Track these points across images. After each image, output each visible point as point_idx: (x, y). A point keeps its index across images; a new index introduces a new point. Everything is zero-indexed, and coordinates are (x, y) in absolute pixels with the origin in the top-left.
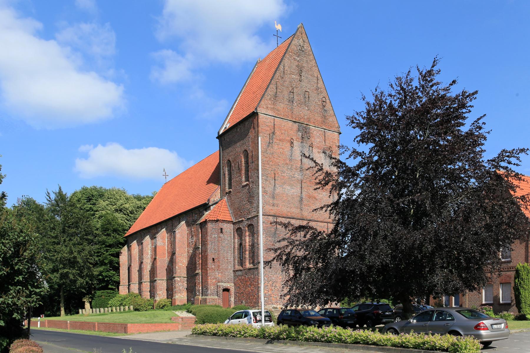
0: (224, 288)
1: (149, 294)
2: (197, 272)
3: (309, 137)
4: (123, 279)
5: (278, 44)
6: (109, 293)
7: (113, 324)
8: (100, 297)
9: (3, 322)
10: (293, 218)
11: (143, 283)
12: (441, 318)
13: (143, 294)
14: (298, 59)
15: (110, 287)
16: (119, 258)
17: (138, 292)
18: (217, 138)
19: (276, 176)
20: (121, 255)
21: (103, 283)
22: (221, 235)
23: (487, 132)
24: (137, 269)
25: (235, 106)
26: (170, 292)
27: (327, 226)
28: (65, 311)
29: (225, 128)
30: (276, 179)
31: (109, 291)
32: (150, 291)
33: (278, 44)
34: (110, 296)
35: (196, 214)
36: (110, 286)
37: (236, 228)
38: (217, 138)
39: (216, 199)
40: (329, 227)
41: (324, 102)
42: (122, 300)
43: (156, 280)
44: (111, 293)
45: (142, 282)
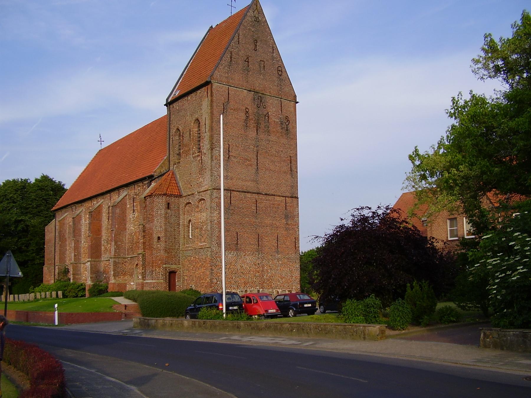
0: (171, 270)
2: (316, 308)
3: (265, 107)
5: (231, 13)
7: (60, 237)
9: (37, 288)
10: (248, 192)
14: (253, 30)
18: (165, 105)
19: (230, 147)
22: (169, 211)
23: (369, 207)
25: (185, 73)
26: (105, 275)
27: (285, 201)
29: (174, 95)
30: (230, 150)
33: (231, 13)
35: (139, 186)
37: (185, 203)
38: (165, 105)
39: (162, 171)
40: (287, 202)
41: (280, 71)
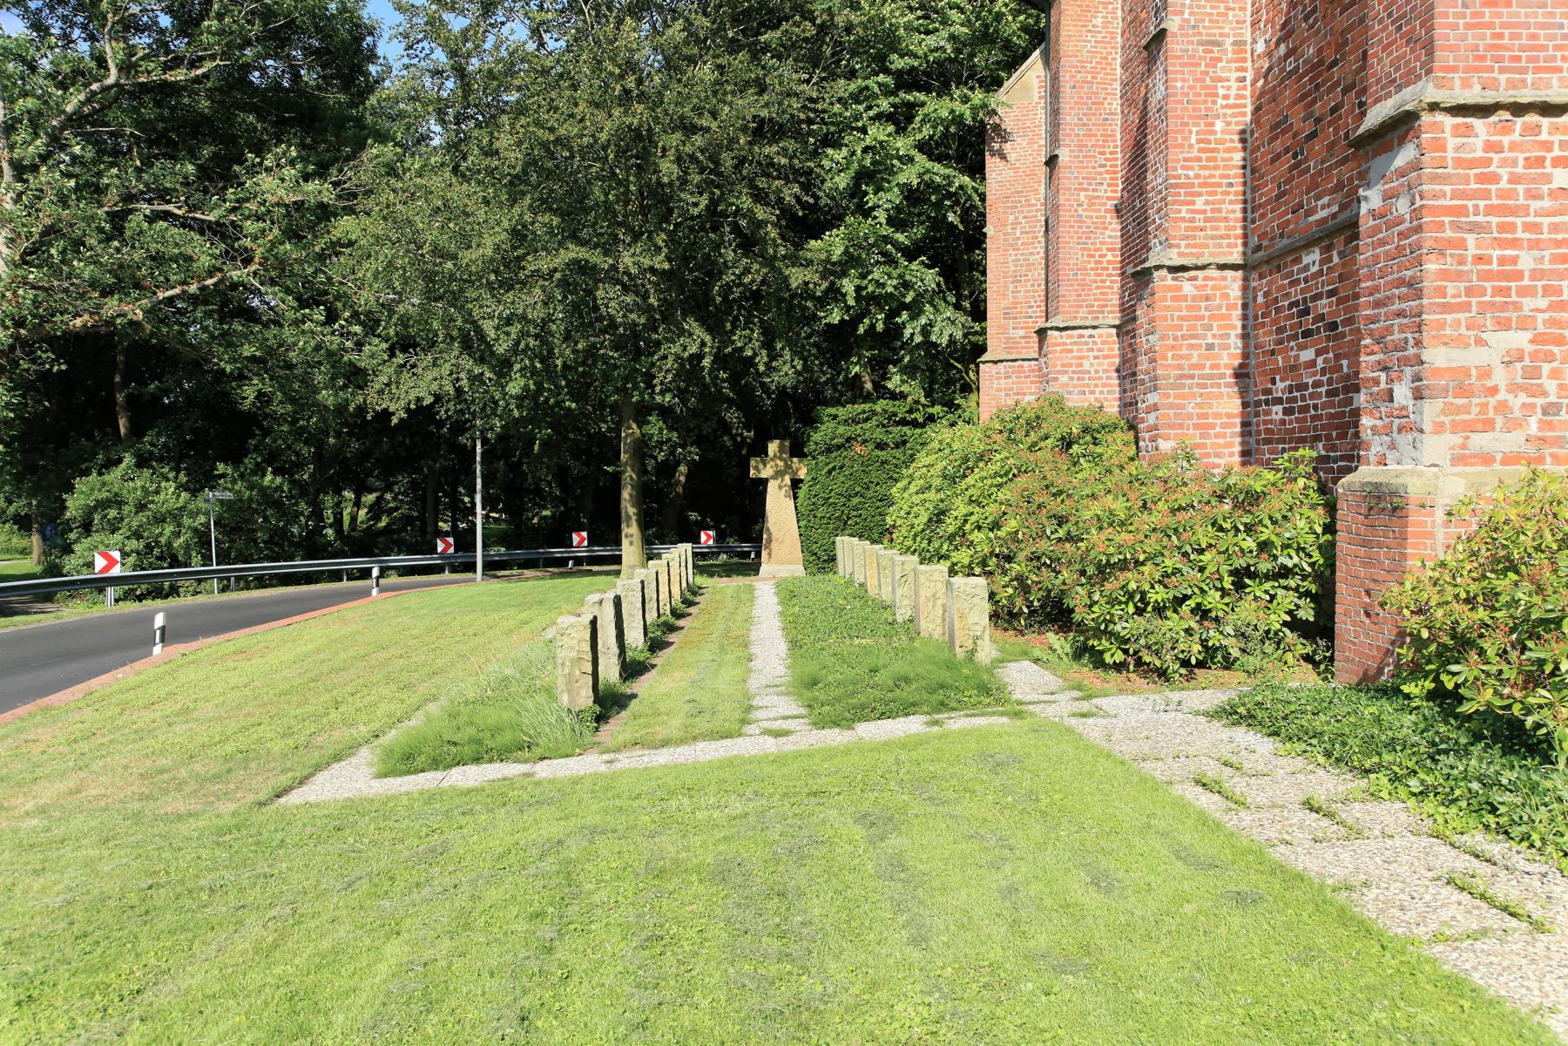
1: (1235, 405)
4: (1006, 316)
6: (903, 422)
8: (839, 447)
11: (1162, 280)
13: (1159, 405)
16: (977, 170)
17: (1112, 408)
24: (1111, 189)
28: (644, 526)
32: (1241, 375)
43: (1402, 125)
45: (1147, 273)
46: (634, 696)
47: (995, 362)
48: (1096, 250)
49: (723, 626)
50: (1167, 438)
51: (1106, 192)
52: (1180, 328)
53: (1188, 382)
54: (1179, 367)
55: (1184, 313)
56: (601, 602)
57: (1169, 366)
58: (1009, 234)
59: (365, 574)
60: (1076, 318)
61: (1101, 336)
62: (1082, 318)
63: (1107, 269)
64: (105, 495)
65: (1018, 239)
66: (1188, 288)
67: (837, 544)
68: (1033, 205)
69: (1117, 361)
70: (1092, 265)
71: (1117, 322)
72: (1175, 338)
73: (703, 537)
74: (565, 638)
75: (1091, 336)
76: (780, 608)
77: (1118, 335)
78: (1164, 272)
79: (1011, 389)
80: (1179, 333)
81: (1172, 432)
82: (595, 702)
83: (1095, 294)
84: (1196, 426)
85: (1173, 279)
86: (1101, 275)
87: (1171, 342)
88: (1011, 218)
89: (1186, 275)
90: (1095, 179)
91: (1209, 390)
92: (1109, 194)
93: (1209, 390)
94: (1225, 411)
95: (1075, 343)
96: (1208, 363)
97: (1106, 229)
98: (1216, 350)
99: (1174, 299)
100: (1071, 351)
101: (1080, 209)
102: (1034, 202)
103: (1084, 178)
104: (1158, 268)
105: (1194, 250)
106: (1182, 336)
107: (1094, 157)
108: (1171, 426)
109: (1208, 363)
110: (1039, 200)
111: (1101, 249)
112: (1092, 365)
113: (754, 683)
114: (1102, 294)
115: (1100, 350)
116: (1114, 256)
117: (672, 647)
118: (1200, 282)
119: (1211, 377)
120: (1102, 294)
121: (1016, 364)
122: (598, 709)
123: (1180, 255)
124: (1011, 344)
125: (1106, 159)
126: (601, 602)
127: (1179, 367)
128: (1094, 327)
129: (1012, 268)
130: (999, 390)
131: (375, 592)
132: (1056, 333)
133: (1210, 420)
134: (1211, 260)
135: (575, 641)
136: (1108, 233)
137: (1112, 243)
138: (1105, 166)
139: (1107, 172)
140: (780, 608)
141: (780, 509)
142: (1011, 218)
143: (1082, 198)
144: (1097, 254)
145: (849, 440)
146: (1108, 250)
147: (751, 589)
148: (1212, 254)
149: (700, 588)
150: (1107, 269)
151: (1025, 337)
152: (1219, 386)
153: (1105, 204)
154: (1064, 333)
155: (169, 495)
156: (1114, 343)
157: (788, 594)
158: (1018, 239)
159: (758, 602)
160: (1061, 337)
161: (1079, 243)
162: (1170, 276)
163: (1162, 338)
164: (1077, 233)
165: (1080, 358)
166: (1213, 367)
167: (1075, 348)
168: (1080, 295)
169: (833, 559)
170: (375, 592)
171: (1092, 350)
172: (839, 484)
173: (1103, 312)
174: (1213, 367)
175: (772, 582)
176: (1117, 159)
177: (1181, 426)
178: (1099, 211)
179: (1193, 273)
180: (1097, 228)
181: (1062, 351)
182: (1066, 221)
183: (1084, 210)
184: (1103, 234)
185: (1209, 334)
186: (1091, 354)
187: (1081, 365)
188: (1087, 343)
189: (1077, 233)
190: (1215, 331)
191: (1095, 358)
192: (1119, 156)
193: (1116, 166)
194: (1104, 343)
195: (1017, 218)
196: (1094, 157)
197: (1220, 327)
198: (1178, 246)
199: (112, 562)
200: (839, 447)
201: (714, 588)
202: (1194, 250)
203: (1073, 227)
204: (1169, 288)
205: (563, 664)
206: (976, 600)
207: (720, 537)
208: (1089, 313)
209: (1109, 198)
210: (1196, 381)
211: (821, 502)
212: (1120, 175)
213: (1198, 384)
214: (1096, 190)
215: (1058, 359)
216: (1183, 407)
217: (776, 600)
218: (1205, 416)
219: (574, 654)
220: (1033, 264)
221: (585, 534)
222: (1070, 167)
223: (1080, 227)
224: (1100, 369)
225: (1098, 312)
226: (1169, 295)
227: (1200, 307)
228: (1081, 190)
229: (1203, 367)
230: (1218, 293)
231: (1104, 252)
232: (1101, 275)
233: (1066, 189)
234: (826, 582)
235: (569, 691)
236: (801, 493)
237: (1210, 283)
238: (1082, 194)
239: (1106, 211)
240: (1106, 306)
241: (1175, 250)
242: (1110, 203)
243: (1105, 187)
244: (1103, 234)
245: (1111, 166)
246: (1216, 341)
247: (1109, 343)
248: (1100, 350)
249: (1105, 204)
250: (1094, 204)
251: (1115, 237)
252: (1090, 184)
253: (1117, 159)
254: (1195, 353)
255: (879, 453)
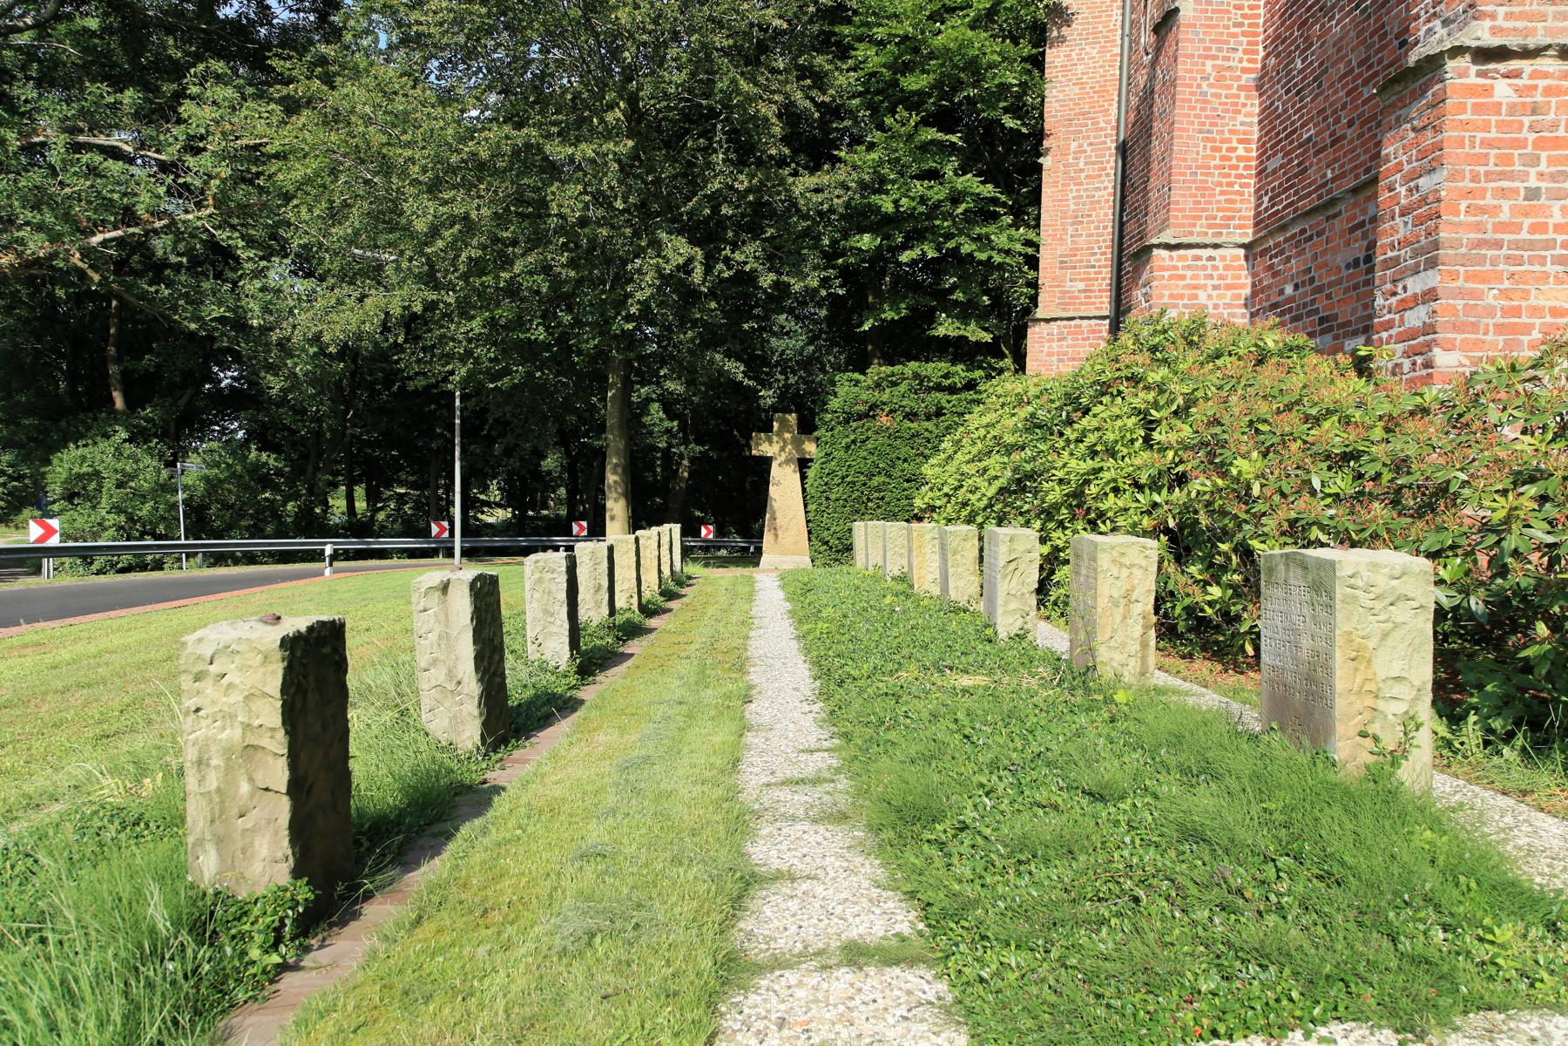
6: (939, 388)
8: (860, 417)
11: (1461, 73)
12: (531, 513)
15: (941, 331)
20: (1062, 39)
21: (895, 307)
31: (934, 369)
34: (939, 413)
36: (946, 327)
42: (1033, 424)
44: (952, 390)
46: (498, 790)
47: (1047, 321)
48: (1222, 141)
49: (708, 631)
50: (1449, 347)
51: (1241, 61)
52: (1483, 159)
53: (1490, 253)
54: (1479, 227)
55: (1493, 134)
56: (445, 588)
57: (1460, 224)
58: (1069, 165)
59: (317, 556)
60: (1191, 233)
61: (1223, 258)
62: (1199, 234)
63: (1236, 168)
64: (85, 469)
65: (1082, 171)
66: (1503, 90)
67: (855, 531)
68: (1101, 129)
69: (1248, 291)
70: (1217, 162)
71: (1247, 240)
72: (1475, 178)
73: (704, 531)
74: (208, 686)
75: (1211, 258)
76: (789, 606)
77: (1247, 258)
78: (1464, 62)
79: (1065, 354)
80: (1482, 169)
81: (1460, 337)
82: (297, 873)
83: (1218, 202)
84: (1500, 329)
85: (1480, 74)
86: (1229, 175)
87: (1467, 184)
88: (1074, 146)
89: (1502, 67)
90: (1227, 42)
91: (1526, 267)
92: (1245, 64)
93: (1526, 267)
94: (1549, 304)
95: (1189, 267)
96: (1527, 222)
97: (1239, 112)
98: (1543, 200)
99: (1478, 108)
100: (1183, 278)
101: (1204, 85)
102: (1103, 125)
103: (1212, 41)
104: (1457, 51)
105: (1519, 24)
106: (1487, 174)
107: (1228, 12)
108: (1456, 328)
109: (1527, 222)
110: (1108, 122)
111: (1229, 141)
112: (1210, 297)
113: (753, 777)
114: (1227, 201)
115: (1221, 277)
116: (1247, 150)
117: (629, 663)
118: (1524, 81)
119: (1531, 245)
120: (1227, 201)
121: (1072, 323)
122: (304, 893)
123: (1495, 31)
124: (1068, 298)
125: (1244, 16)
126: (445, 588)
127: (1479, 227)
128: (1216, 246)
129: (1073, 207)
130: (1050, 354)
131: (327, 572)
132: (1164, 253)
133: (1524, 319)
134: (1548, 41)
135: (236, 697)
136: (1241, 118)
137: (1245, 133)
138: (1241, 25)
139: (1244, 34)
140: (789, 606)
141: (785, 488)
142: (1074, 146)
143: (1209, 69)
144: (1225, 146)
145: (873, 407)
146: (1240, 141)
147: (751, 582)
148: (1548, 32)
149: (690, 578)
150: (1236, 168)
151: (1085, 291)
152: (1543, 260)
153: (1239, 78)
154: (1175, 253)
155: (149, 468)
156: (1241, 268)
157: (800, 592)
158: (1082, 171)
159: (758, 597)
160: (1171, 258)
161: (1201, 132)
162: (1474, 69)
163: (1452, 178)
164: (1199, 116)
165: (1195, 287)
166: (1534, 228)
167: (1189, 273)
168: (1199, 203)
169: (849, 548)
170: (327, 572)
171: (1211, 277)
172: (860, 460)
173: (1228, 226)
174: (1534, 228)
175: (775, 574)
176: (1258, 16)
177: (1474, 327)
178: (1229, 87)
179: (1514, 64)
180: (1227, 111)
181: (1171, 278)
182: (1184, 100)
183: (1210, 85)
184: (1235, 119)
185: (1533, 171)
186: (1210, 282)
187: (1195, 297)
188: (1205, 268)
189: (1199, 116)
190: (1543, 167)
191: (1215, 288)
192: (1262, 11)
193: (1257, 25)
194: (1226, 268)
195: (1081, 146)
196: (1228, 12)
197: (1550, 161)
198: (1493, 16)
199: (50, 531)
200: (860, 417)
201: (706, 578)
202: (1519, 24)
203: (1194, 108)
204: (1471, 91)
205: (200, 763)
206: (1401, 613)
207: (720, 532)
208: (1210, 227)
209: (1244, 70)
210: (1504, 251)
211: (836, 480)
212: (1261, 38)
213: (1508, 257)
214: (1228, 59)
215: (1165, 287)
216: (1478, 295)
217: (781, 595)
218: (1516, 311)
219: (232, 734)
220: (1099, 202)
221: (584, 524)
222: (1194, 26)
223: (1203, 109)
224: (1220, 303)
225: (1221, 226)
226: (1470, 101)
227: (1521, 124)
228: (1207, 57)
229: (1517, 228)
230: (1554, 100)
231: (1234, 144)
232: (1229, 175)
233: (1185, 56)
234: (839, 576)
235: (220, 841)
236: (811, 473)
237: (1542, 83)
238: (1209, 63)
239: (1240, 88)
240: (1232, 218)
241: (1487, 23)
242: (1245, 76)
243: (1240, 54)
244: (1235, 119)
245: (1250, 25)
246: (1543, 185)
247: (1234, 268)
248: (1221, 277)
249: (1239, 78)
250: (1223, 78)
251: (1251, 124)
252: (1220, 50)
253: (1258, 16)
254: (1506, 205)
255: (907, 424)
